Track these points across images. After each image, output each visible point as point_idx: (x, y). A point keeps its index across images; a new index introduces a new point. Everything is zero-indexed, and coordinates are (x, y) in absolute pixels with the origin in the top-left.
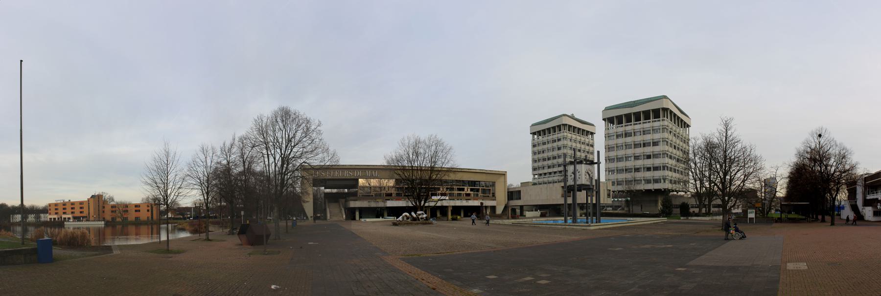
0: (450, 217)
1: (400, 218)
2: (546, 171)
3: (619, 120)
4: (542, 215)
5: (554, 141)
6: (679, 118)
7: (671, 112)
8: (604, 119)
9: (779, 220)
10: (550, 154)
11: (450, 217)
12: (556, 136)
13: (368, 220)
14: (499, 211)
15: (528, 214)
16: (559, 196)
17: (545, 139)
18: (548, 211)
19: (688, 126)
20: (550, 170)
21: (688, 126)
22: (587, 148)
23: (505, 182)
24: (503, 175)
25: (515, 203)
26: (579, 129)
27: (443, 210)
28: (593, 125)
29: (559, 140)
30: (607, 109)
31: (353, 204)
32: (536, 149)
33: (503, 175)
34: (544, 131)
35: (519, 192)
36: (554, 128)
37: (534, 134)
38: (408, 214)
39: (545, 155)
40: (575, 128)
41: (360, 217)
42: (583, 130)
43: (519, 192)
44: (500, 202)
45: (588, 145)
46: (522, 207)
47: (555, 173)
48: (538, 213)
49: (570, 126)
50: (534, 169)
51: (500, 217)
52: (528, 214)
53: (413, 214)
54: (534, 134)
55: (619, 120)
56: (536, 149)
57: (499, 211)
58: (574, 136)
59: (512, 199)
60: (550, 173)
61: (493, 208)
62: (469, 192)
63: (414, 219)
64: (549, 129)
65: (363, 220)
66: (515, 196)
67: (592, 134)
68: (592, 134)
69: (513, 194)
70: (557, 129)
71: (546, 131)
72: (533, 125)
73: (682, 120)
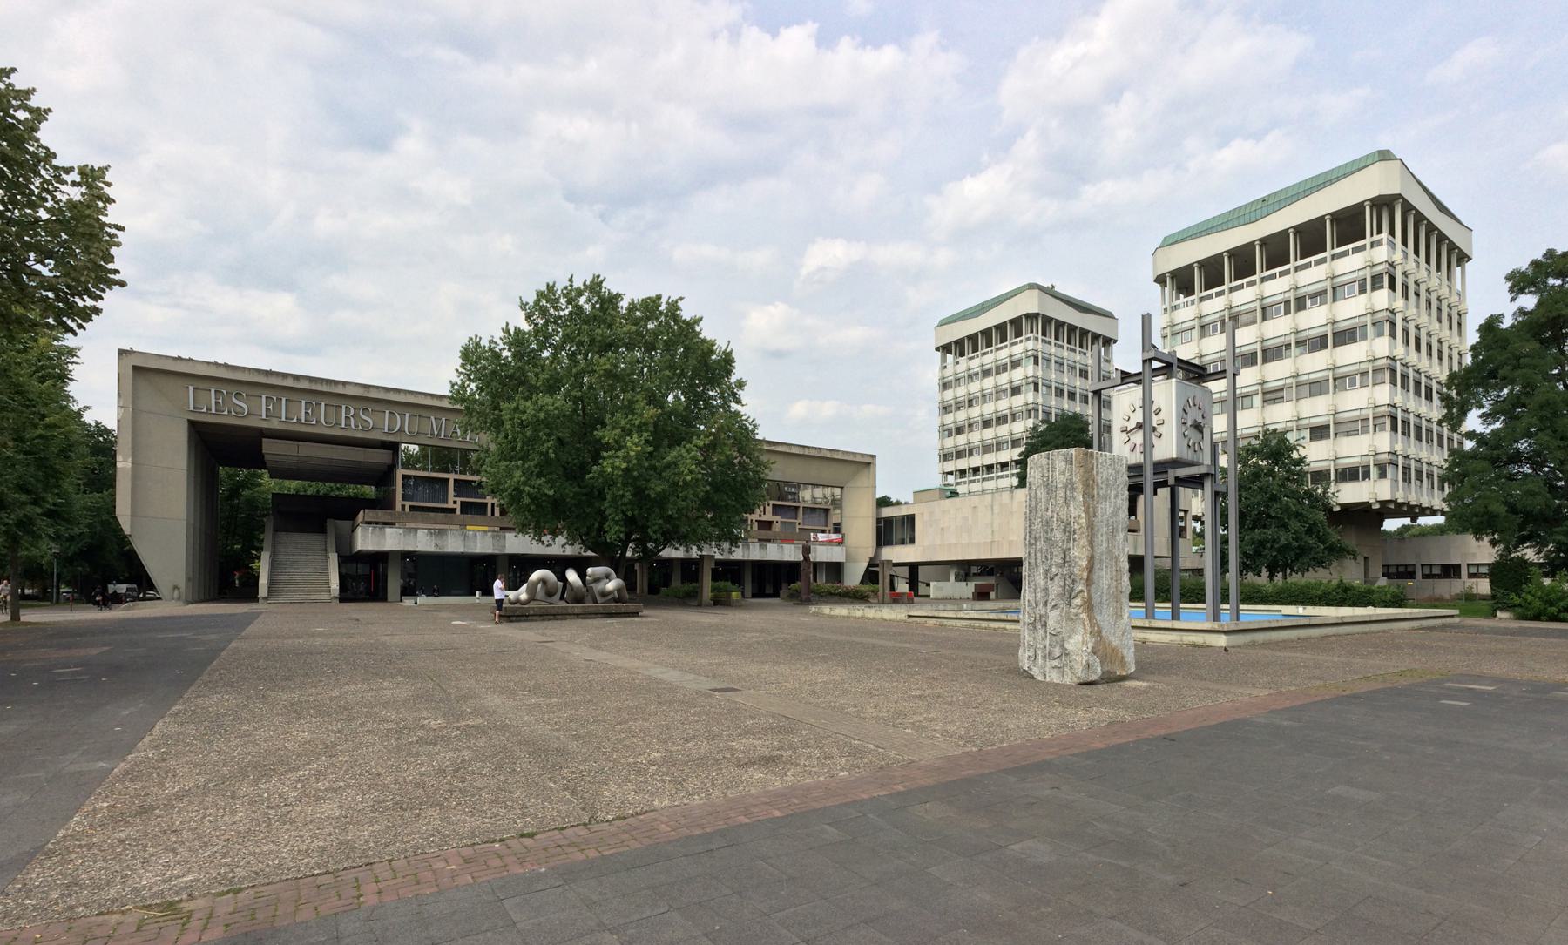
0: (707, 593)
2: (976, 461)
3: (1211, 273)
5: (1002, 369)
6: (1431, 228)
7: (1408, 207)
8: (1160, 280)
10: (989, 409)
14: (854, 577)
15: (935, 589)
18: (991, 580)
19: (1463, 258)
20: (990, 459)
21: (1463, 258)
24: (864, 464)
25: (897, 554)
26: (1072, 329)
27: (690, 569)
28: (1109, 315)
31: (367, 540)
34: (973, 338)
36: (1001, 328)
37: (946, 349)
40: (1060, 324)
41: (407, 591)
42: (1084, 333)
46: (913, 568)
48: (968, 589)
51: (856, 597)
52: (935, 589)
53: (572, 576)
55: (1211, 273)
57: (854, 577)
59: (889, 543)
60: (990, 468)
61: (836, 569)
62: (768, 517)
64: (986, 333)
65: (408, 602)
66: (897, 535)
67: (1108, 342)
68: (1108, 342)
70: (1010, 331)
72: (943, 323)
73: (1442, 238)
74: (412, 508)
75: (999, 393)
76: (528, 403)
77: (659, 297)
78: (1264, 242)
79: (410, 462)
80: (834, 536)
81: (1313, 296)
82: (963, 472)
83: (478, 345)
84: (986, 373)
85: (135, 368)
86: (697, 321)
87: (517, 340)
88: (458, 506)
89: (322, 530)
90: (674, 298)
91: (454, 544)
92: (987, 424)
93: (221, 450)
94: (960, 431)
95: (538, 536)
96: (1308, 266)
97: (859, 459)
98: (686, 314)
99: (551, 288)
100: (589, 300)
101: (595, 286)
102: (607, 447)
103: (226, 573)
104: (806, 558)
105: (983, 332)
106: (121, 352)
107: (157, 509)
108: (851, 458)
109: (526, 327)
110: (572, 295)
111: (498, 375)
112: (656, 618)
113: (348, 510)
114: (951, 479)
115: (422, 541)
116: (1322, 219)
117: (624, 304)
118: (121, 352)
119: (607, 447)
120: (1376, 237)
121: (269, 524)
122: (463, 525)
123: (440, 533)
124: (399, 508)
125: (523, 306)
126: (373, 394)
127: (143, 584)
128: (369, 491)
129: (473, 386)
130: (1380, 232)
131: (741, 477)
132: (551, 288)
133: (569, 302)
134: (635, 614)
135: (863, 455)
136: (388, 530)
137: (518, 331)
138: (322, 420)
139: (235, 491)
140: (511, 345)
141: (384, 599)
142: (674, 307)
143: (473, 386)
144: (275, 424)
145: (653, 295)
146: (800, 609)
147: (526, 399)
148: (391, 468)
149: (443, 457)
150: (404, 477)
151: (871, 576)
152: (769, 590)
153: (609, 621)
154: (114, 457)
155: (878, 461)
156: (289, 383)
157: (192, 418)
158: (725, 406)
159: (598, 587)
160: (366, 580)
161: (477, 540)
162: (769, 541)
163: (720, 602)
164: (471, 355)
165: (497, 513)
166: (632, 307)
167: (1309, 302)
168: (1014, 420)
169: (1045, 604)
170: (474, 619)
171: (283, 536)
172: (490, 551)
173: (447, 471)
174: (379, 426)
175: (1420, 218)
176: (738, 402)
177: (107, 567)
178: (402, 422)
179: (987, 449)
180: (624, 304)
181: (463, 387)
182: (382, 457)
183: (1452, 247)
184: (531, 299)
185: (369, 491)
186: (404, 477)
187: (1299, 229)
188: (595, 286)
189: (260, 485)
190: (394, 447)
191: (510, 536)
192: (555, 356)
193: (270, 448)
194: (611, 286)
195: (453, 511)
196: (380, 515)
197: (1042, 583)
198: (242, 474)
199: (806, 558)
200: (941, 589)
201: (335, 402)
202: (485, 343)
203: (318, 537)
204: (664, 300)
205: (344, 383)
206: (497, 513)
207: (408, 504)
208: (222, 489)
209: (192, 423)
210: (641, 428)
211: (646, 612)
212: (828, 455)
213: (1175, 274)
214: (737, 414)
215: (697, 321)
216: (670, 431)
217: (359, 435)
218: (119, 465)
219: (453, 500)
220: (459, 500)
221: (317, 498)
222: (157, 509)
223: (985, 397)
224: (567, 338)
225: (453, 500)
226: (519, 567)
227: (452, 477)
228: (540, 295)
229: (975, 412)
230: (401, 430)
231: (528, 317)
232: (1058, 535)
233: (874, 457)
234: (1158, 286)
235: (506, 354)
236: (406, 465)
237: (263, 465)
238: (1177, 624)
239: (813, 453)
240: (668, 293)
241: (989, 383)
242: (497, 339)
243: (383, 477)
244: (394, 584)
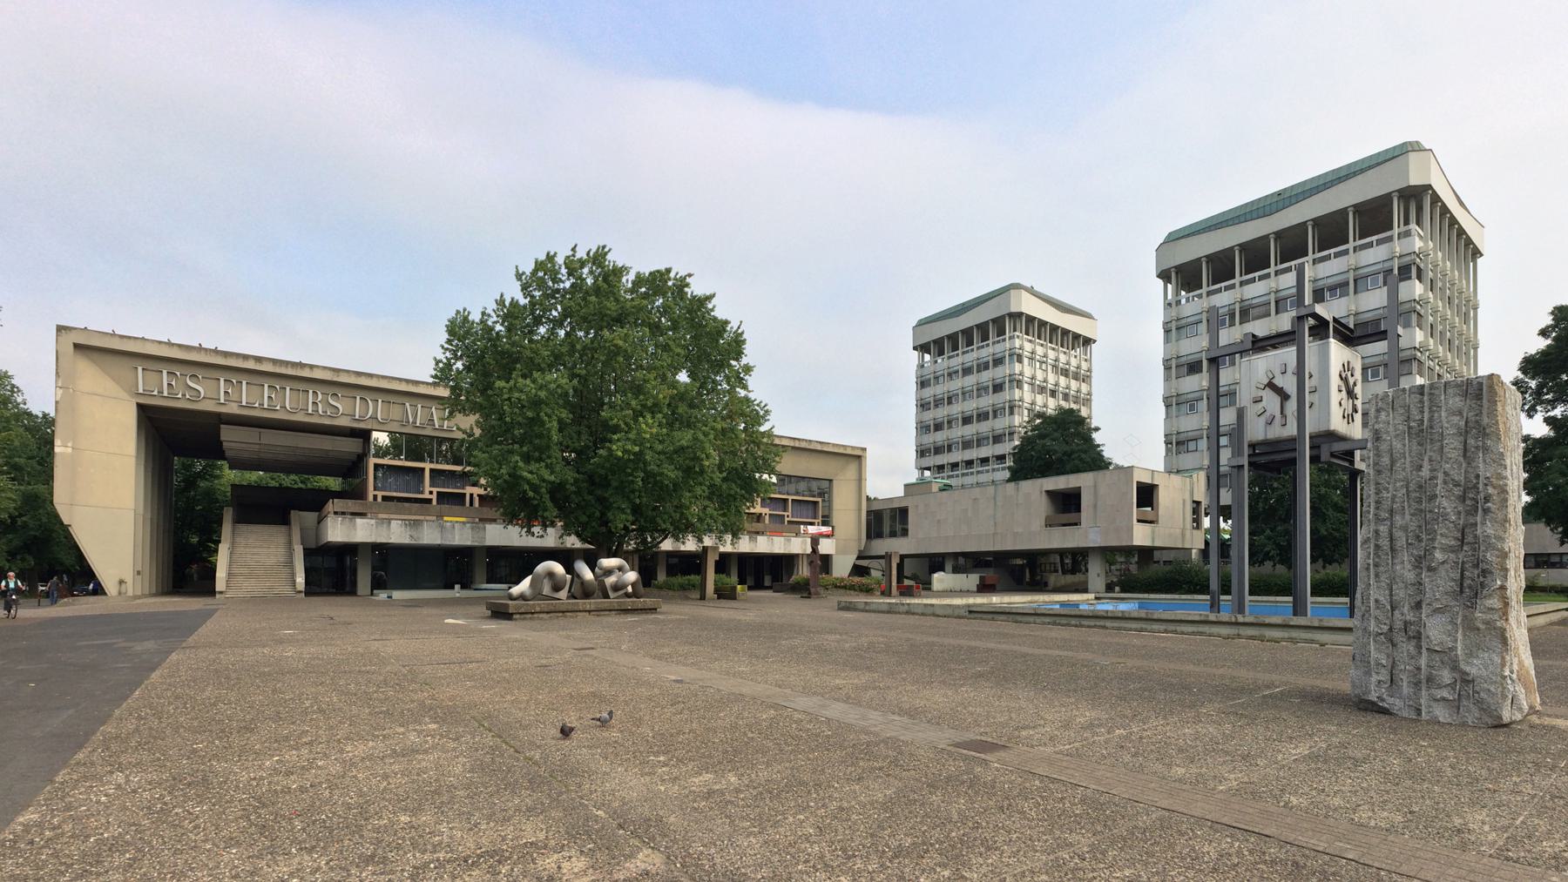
0: (1308, 571)
1: (524, 585)
2: (957, 456)
3: (1221, 267)
4: (985, 588)
5: (984, 366)
7: (1436, 199)
9: (669, 587)
10: (971, 406)
11: (1308, 571)
12: (986, 352)
13: (398, 595)
16: (1038, 523)
17: (957, 361)
19: (1477, 253)
21: (1477, 253)
22: (1074, 384)
23: (860, 480)
24: (856, 458)
25: (898, 546)
26: (1054, 328)
27: (690, 564)
28: (1089, 316)
29: (998, 362)
30: (1174, 238)
31: (337, 531)
32: (928, 393)
33: (856, 458)
35: (903, 513)
38: (558, 568)
39: (957, 409)
40: (1043, 324)
41: (378, 584)
42: (1065, 332)
43: (903, 513)
44: (841, 544)
45: (1076, 377)
47: (985, 461)
48: (972, 580)
49: (1031, 319)
50: (922, 452)
54: (922, 348)
55: (1221, 267)
56: (928, 393)
58: (1040, 351)
59: (879, 535)
60: (969, 463)
63: (586, 592)
65: (382, 595)
67: (1088, 342)
69: (885, 520)
71: (966, 339)
73: (1461, 232)
74: (385, 498)
75: (981, 390)
76: (528, 381)
77: (668, 271)
78: (1279, 235)
79: (382, 452)
80: (824, 529)
81: (1332, 289)
82: (941, 468)
83: (466, 319)
84: (967, 371)
85: (77, 346)
86: (710, 298)
87: (511, 314)
88: (434, 497)
89: (284, 521)
90: (682, 273)
91: (430, 536)
92: (967, 420)
93: (179, 444)
94: (938, 427)
95: (528, 527)
96: (1328, 258)
97: (849, 451)
98: (696, 288)
99: (550, 258)
100: (591, 272)
101: (599, 257)
102: (616, 429)
103: (184, 564)
104: (814, 550)
105: (949, 337)
106: (60, 329)
107: (104, 499)
108: (841, 451)
109: (523, 301)
110: (573, 266)
111: (486, 357)
112: (677, 611)
113: (316, 502)
114: (927, 473)
115: (396, 533)
116: (1344, 212)
117: (628, 279)
118: (60, 329)
119: (616, 429)
120: (1403, 228)
121: (228, 515)
122: (440, 517)
123: (416, 524)
124: (371, 498)
125: (519, 276)
126: (344, 379)
127: (82, 578)
128: (333, 483)
129: (459, 365)
130: (1407, 223)
131: (743, 467)
132: (550, 258)
133: (570, 274)
134: (653, 610)
135: (853, 448)
136: (359, 521)
137: (514, 303)
138: (288, 405)
139: (190, 482)
140: (505, 318)
141: (352, 592)
142: (682, 284)
143: (459, 365)
144: (232, 409)
145: (662, 268)
146: (807, 601)
147: (524, 377)
148: (361, 458)
149: (413, 445)
150: (377, 466)
151: (858, 570)
152: (767, 582)
153: (631, 618)
154: (52, 443)
156: (251, 365)
157: (142, 401)
158: (731, 392)
159: (610, 580)
160: (333, 572)
161: (456, 531)
162: (758, 533)
163: (725, 594)
164: (459, 329)
165: (476, 503)
166: (639, 281)
167: (1327, 294)
168: (995, 416)
169: (1418, 606)
170: (466, 617)
171: (243, 527)
172: (469, 543)
173: (422, 460)
174: (345, 412)
175: (1445, 210)
176: (745, 387)
177: (57, 564)
178: (378, 409)
179: (967, 445)
180: (628, 279)
181: (449, 365)
182: (351, 446)
183: (1469, 242)
184: (528, 268)
185: (333, 483)
186: (377, 466)
187: (1210, 258)
188: (599, 257)
189: (218, 477)
190: (365, 435)
191: (489, 527)
192: (552, 332)
193: (228, 435)
194: (615, 258)
195: (429, 501)
196: (351, 505)
197: (1410, 576)
198: (199, 466)
199: (814, 550)
201: (301, 386)
202: (475, 317)
203: (283, 528)
204: (672, 275)
205: (312, 367)
206: (476, 503)
207: (380, 494)
208: (177, 480)
209: (140, 407)
210: (654, 409)
211: (665, 608)
213: (1180, 269)
214: (747, 399)
215: (710, 298)
216: (681, 409)
217: (327, 422)
218: (57, 450)
219: (429, 491)
220: (435, 490)
221: (281, 489)
222: (104, 499)
223: (966, 394)
224: (566, 314)
225: (429, 491)
226: (519, 562)
227: (427, 466)
228: (539, 266)
229: (957, 409)
230: (374, 418)
231: (524, 288)
232: (1447, 505)
233: (864, 449)
234: (1161, 282)
235: (498, 327)
236: (377, 455)
237: (224, 458)
238: (1241, 619)
239: (803, 445)
240: (679, 270)
241: (970, 381)
242: (489, 311)
243: (352, 469)
244: (364, 578)
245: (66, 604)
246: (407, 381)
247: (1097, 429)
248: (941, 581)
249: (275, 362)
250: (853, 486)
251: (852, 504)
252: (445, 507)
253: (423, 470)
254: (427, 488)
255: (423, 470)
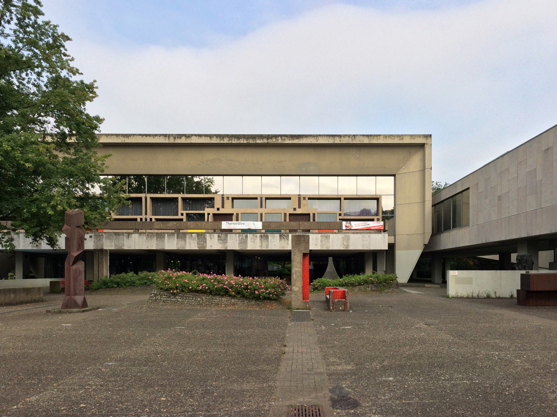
14: (406, 263)
23: (424, 170)
74: (157, 220)
88: (184, 217)
97: (407, 141)
108: (396, 141)
155: (434, 141)
172: (197, 249)
195: (182, 220)
200: (469, 281)
207: (154, 218)
212: (366, 141)
219: (182, 212)
225: (182, 212)
227: (180, 196)
239: (345, 141)
245: (107, 296)
246: (142, 135)
247: (97, 88)
248: (459, 281)
249: (385, 136)
250: (416, 178)
251: (416, 196)
252: (191, 223)
253: (177, 198)
254: (180, 211)
255: (177, 198)
